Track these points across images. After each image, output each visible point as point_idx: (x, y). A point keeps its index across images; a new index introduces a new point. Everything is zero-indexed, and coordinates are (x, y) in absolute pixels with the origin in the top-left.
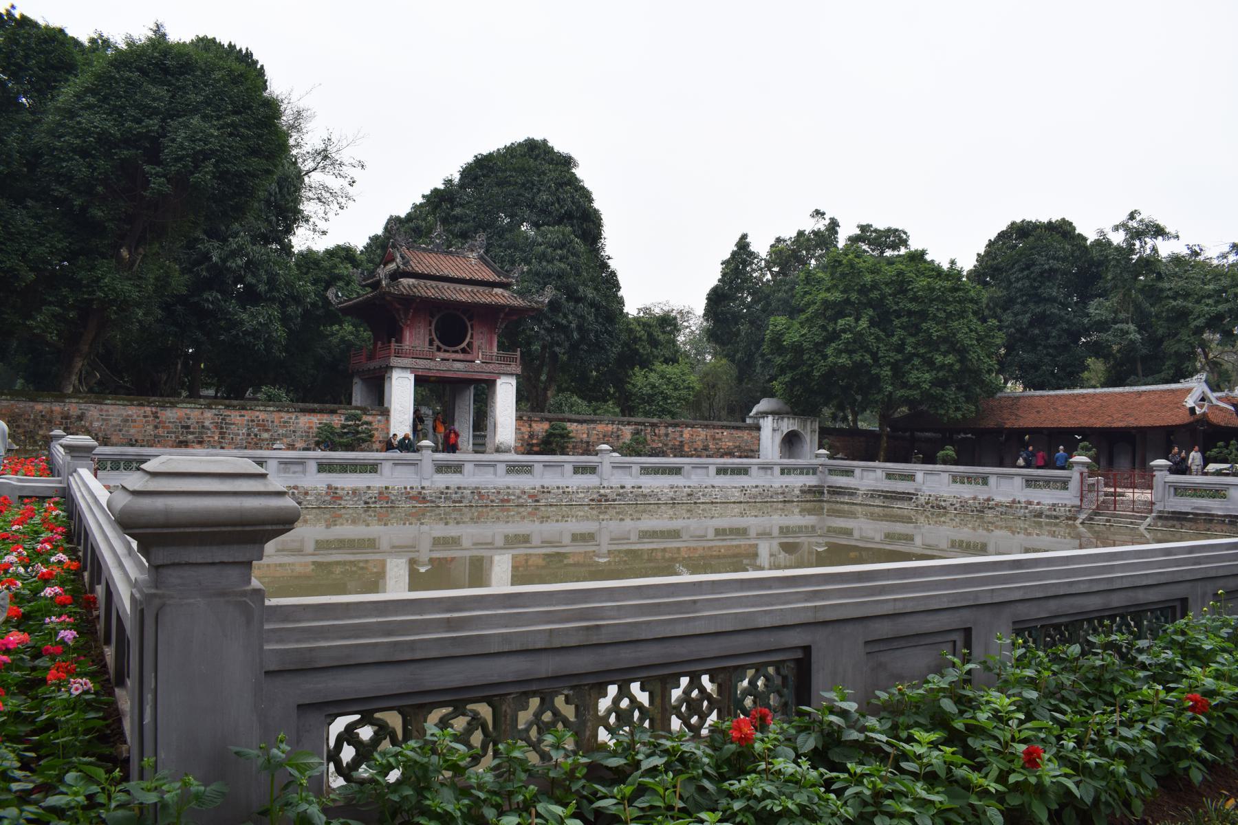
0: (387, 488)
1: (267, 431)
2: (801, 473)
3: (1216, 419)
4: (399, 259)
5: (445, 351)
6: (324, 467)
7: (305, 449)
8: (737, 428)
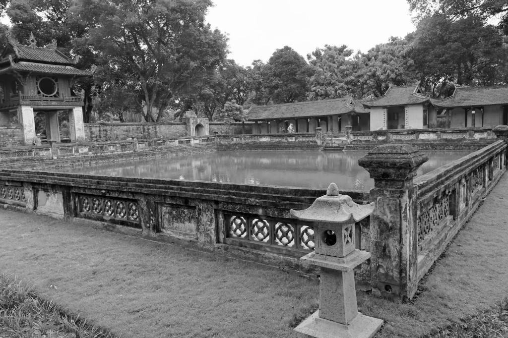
5: (46, 96)
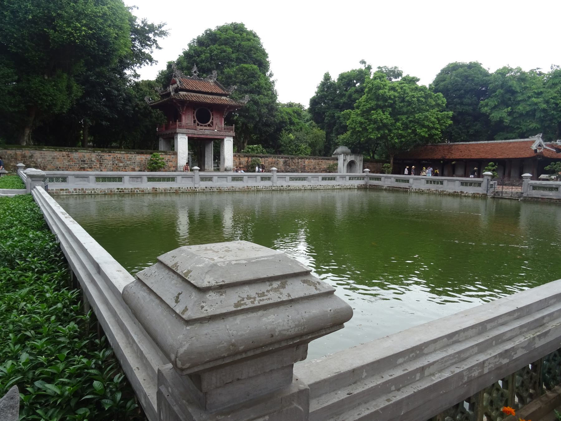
0: (179, 188)
1: (122, 162)
2: (358, 179)
3: (546, 154)
4: (178, 83)
5: (201, 126)
6: (150, 179)
7: (140, 171)
8: (328, 159)
